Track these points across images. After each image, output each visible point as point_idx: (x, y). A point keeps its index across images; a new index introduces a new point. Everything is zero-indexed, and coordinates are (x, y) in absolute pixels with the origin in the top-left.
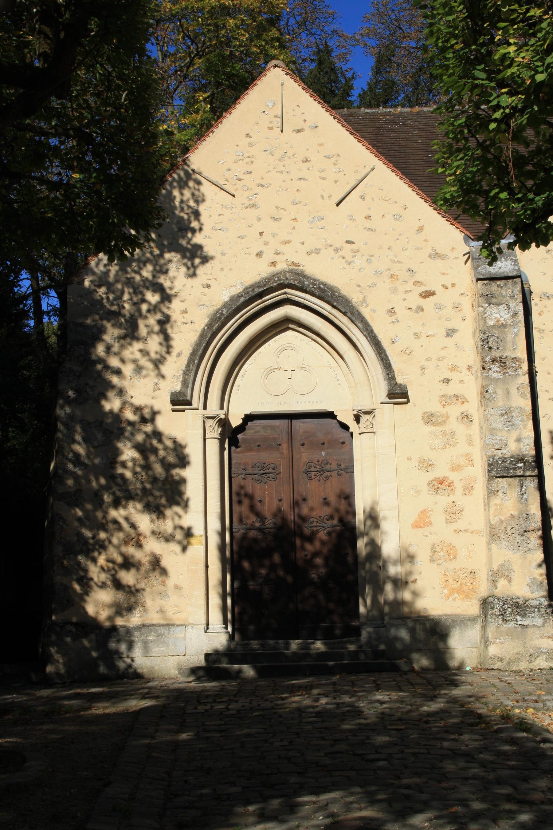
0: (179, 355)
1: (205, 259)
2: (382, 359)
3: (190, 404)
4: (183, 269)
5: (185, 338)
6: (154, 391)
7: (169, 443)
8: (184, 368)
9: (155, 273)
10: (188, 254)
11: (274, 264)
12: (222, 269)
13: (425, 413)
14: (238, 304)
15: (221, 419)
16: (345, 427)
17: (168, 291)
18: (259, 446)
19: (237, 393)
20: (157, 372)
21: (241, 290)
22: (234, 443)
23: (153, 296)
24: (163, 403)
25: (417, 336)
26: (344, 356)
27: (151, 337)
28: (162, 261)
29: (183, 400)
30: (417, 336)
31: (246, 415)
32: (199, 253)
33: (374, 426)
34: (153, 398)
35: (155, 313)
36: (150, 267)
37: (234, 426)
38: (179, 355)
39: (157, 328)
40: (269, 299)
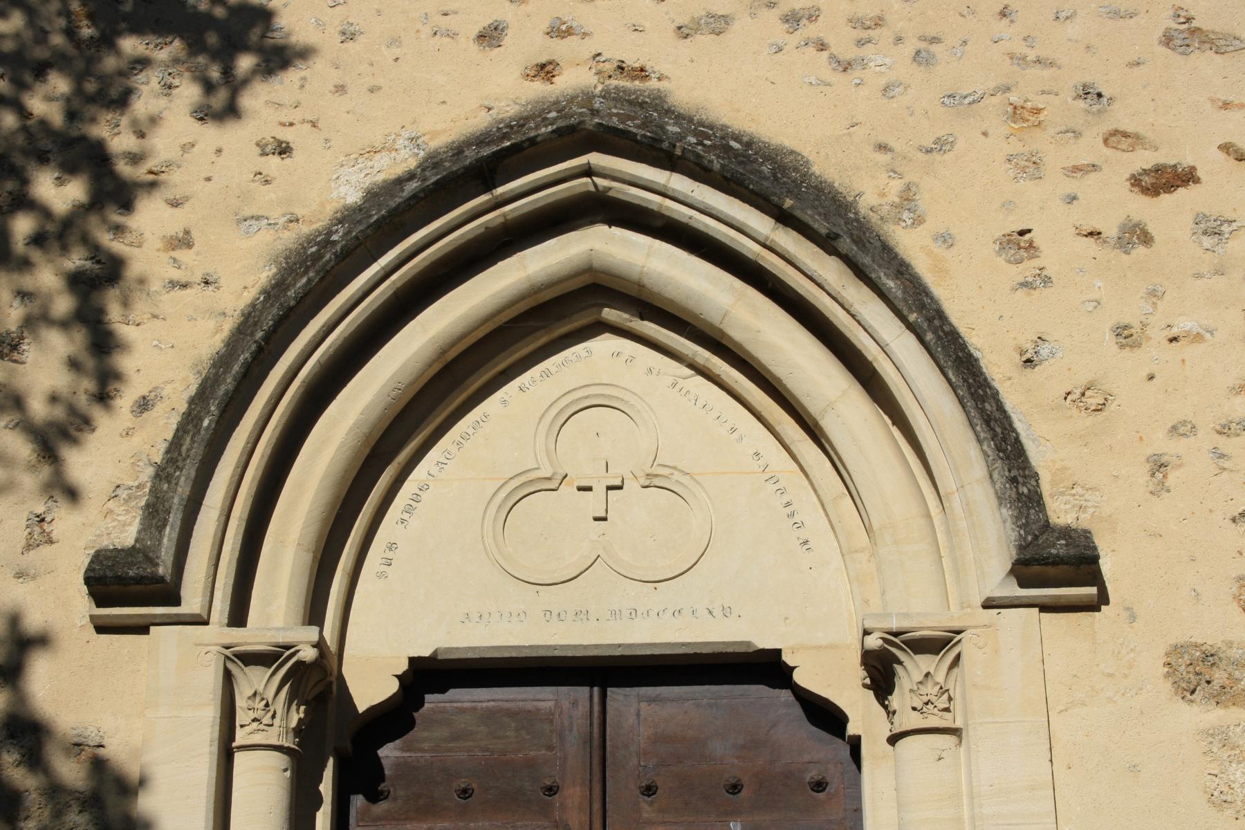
0: (144, 405)
1: (279, 58)
2: (987, 421)
3: (177, 602)
4: (189, 92)
5: (169, 346)
6: (29, 547)
7: (71, 772)
8: (158, 458)
9: (76, 104)
10: (212, 39)
11: (545, 70)
12: (340, 89)
13: (1177, 649)
14: (393, 204)
15: (300, 663)
16: (827, 717)
17: (124, 169)
18: (465, 793)
19: (381, 575)
20: (46, 471)
21: (412, 164)
22: (362, 778)
23: (60, 182)
24: (57, 599)
25: (1125, 335)
26: (829, 425)
27: (37, 339)
28: (110, 63)
29: (139, 580)
30: (1125, 335)
31: (412, 660)
32: (254, 35)
33: (957, 705)
34: (20, 575)
35: (65, 249)
36: (60, 84)
37: (362, 707)
38: (144, 405)
39: (63, 305)
40: (525, 192)
